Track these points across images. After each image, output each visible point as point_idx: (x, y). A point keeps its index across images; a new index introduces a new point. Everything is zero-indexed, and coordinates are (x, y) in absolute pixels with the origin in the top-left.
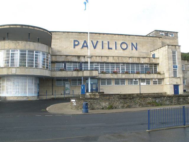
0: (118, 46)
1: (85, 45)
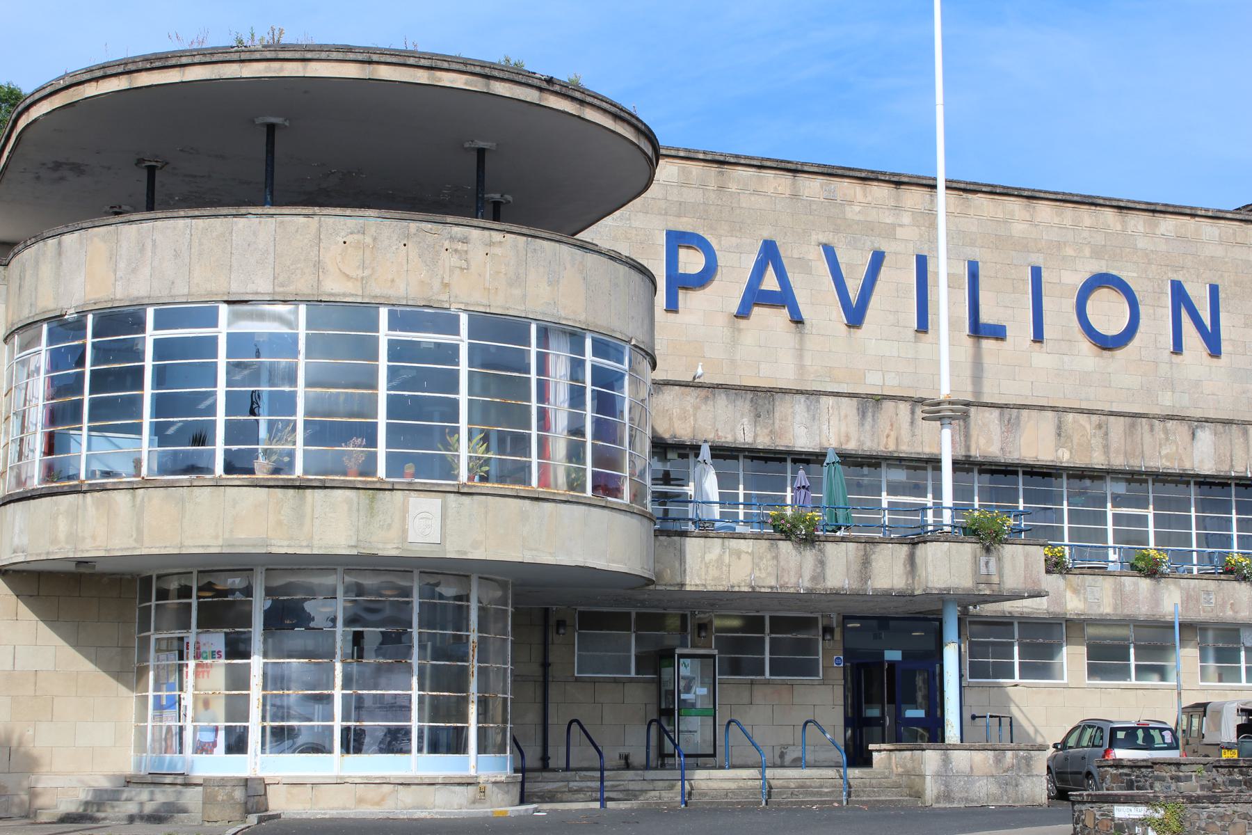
0: (1060, 311)
1: (770, 283)
